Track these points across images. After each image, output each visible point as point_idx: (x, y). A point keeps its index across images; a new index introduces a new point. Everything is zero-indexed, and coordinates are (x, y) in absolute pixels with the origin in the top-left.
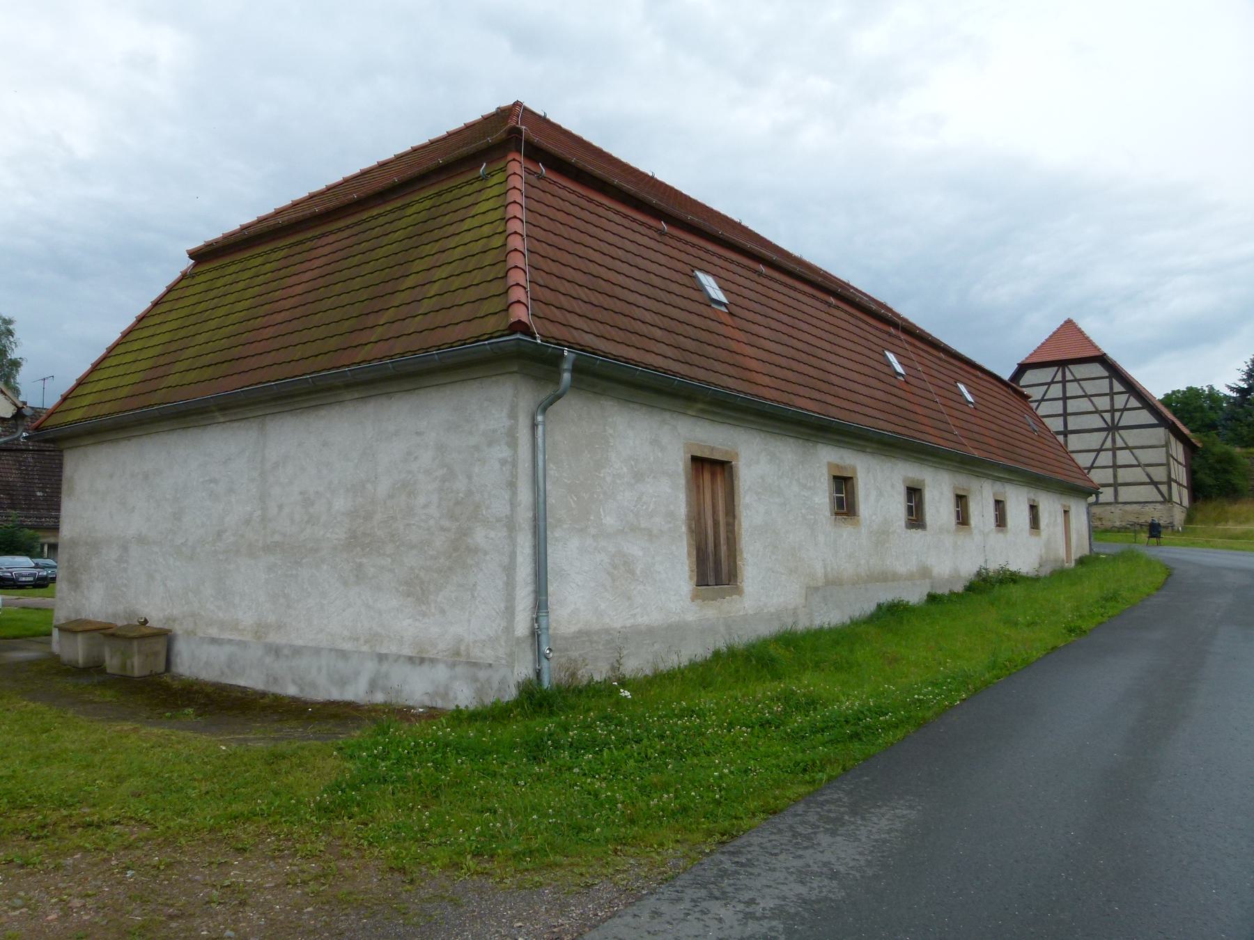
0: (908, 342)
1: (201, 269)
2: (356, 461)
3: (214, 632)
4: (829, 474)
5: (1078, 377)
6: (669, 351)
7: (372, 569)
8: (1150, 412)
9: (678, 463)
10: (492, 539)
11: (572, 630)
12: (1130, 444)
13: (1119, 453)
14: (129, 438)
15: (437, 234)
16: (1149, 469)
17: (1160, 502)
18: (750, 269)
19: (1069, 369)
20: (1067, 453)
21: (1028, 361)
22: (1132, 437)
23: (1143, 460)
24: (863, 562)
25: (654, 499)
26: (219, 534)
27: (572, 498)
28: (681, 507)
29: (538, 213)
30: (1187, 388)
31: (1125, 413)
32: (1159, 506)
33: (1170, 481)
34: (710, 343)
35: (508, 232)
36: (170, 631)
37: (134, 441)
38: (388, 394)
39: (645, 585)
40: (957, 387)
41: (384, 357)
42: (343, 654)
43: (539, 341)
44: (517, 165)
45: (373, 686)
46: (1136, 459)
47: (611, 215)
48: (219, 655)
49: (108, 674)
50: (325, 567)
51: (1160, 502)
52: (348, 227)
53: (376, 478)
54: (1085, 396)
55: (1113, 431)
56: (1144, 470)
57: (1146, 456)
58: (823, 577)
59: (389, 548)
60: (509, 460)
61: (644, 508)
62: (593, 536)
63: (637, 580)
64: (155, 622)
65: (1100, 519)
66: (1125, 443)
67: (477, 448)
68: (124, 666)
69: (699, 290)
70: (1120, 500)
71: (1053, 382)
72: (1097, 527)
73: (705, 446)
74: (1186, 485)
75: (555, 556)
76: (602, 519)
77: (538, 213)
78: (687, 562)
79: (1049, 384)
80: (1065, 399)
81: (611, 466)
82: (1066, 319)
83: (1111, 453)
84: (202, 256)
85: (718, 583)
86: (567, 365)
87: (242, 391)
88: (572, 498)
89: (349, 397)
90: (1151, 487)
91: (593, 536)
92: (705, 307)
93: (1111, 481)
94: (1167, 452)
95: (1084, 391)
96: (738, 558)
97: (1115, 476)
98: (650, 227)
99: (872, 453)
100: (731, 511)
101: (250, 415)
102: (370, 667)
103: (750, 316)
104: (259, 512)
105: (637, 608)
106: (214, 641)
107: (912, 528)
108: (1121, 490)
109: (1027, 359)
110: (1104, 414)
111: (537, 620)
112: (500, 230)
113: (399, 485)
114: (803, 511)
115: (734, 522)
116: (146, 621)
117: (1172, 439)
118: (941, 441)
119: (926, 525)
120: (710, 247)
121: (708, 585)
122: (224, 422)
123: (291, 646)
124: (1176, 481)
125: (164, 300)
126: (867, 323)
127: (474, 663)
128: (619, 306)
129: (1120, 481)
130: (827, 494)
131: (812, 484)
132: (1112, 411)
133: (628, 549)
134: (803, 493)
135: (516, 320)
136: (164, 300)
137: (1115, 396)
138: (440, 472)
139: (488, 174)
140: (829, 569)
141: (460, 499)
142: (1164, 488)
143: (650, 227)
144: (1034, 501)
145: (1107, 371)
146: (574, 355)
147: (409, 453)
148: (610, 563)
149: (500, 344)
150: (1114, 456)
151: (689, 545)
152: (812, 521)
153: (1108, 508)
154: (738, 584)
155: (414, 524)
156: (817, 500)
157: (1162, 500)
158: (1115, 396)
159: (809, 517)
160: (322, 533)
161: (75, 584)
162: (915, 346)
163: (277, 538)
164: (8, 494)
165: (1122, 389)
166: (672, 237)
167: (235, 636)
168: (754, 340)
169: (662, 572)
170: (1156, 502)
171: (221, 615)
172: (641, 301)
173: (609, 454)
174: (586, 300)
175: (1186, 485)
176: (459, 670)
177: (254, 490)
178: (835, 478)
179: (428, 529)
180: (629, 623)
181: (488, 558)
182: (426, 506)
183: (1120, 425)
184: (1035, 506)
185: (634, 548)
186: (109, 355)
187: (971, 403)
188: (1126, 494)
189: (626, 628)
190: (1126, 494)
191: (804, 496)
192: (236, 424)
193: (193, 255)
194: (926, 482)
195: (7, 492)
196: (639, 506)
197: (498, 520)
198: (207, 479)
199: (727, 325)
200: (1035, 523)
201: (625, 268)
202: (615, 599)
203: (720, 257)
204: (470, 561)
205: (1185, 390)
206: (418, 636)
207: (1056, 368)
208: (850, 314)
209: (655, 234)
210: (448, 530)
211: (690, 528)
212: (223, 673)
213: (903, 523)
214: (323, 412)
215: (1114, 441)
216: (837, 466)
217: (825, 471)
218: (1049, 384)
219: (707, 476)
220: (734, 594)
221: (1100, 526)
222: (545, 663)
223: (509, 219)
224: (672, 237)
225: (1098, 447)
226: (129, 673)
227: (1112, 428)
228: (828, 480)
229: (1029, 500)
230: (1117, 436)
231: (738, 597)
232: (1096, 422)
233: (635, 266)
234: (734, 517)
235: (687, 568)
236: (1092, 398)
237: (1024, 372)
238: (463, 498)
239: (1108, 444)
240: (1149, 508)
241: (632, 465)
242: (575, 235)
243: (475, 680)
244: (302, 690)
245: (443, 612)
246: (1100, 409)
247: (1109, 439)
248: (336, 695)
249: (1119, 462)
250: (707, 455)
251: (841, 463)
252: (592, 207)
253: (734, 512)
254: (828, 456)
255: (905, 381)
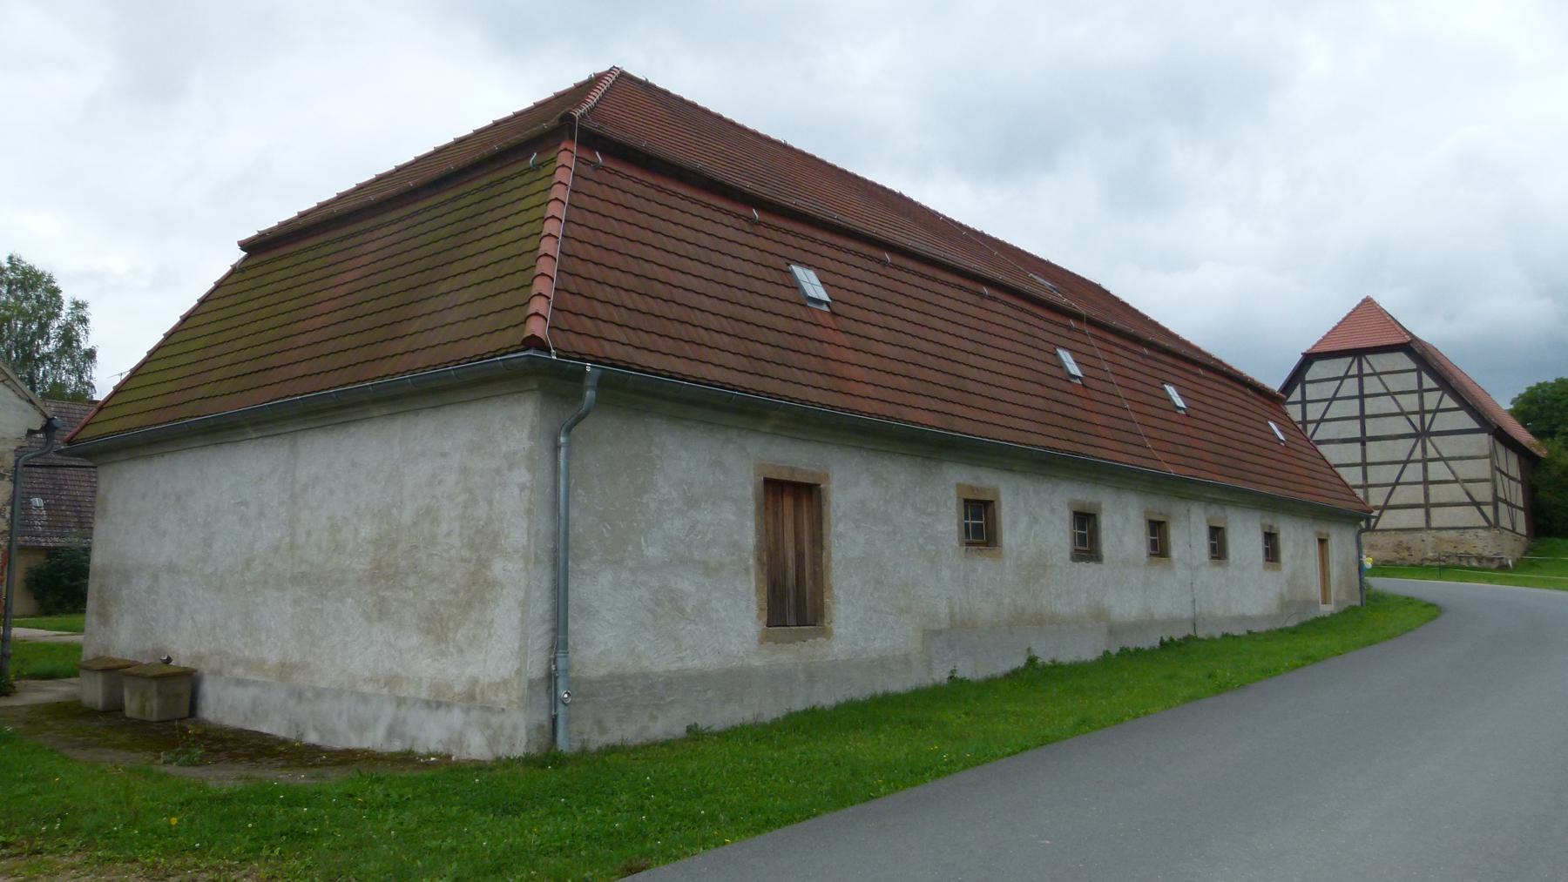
0: (1094, 336)
1: (256, 260)
2: (383, 483)
3: (239, 672)
4: (958, 498)
5: (1378, 370)
6: (732, 361)
7: (395, 604)
8: (1469, 414)
9: (745, 486)
10: (509, 571)
11: (601, 673)
12: (1445, 455)
13: (1430, 465)
14: (162, 455)
15: (481, 232)
16: (1468, 486)
17: (1483, 528)
18: (872, 259)
19: (1366, 359)
20: (1331, 468)
21: (1314, 351)
22: (1447, 446)
23: (1462, 475)
24: (1007, 601)
25: (712, 528)
26: (248, 564)
27: (605, 527)
28: (749, 537)
29: (587, 210)
30: (1557, 380)
31: (1439, 415)
32: (1482, 533)
33: (1496, 500)
34: (797, 349)
35: (543, 234)
36: (196, 671)
37: (167, 457)
38: (416, 411)
39: (697, 625)
40: (1164, 389)
41: (428, 367)
42: (364, 698)
43: (555, 358)
44: (567, 158)
45: (391, 733)
46: (1453, 473)
47: (685, 205)
48: (244, 696)
49: (126, 718)
50: (350, 600)
51: (1483, 528)
52: (400, 220)
53: (402, 503)
54: (1388, 393)
55: (1423, 437)
56: (1462, 486)
57: (1466, 470)
58: (948, 618)
59: (412, 581)
60: (528, 484)
61: (699, 537)
62: (631, 569)
63: (687, 619)
64: (182, 660)
65: (1408, 549)
66: (1439, 453)
67: (498, 471)
68: (142, 709)
69: (793, 287)
70: (1433, 524)
71: (1346, 376)
72: (1403, 559)
73: (783, 467)
74: (1522, 506)
75: (580, 590)
76: (642, 551)
77: (587, 210)
78: (754, 598)
79: (1342, 379)
80: (1362, 397)
81: (657, 491)
82: (1364, 297)
83: (1420, 465)
84: (256, 247)
85: (801, 622)
86: (589, 383)
87: (269, 406)
88: (605, 527)
89: (376, 413)
90: (1473, 509)
91: (631, 569)
92: (799, 307)
93: (1422, 501)
94: (1492, 463)
95: (1386, 388)
96: (826, 595)
97: (1426, 495)
98: (738, 216)
99: (1024, 473)
100: (818, 541)
101: (283, 431)
102: (389, 711)
103: (856, 313)
104: (288, 539)
105: (686, 650)
106: (240, 682)
107: (1082, 561)
108: (1434, 512)
109: (1314, 347)
110: (1412, 417)
111: (555, 660)
112: (537, 231)
113: (424, 510)
114: (921, 541)
115: (822, 553)
116: (169, 660)
117: (1501, 449)
118: (1123, 458)
119: (1102, 556)
120: (819, 235)
121: (786, 626)
122: (257, 438)
123: (314, 688)
124: (1505, 501)
125: (211, 298)
126: (1037, 316)
127: (489, 707)
128: (674, 311)
129: (1432, 500)
130: (955, 521)
131: (934, 509)
132: (1422, 412)
133: (676, 584)
134: (920, 520)
135: (529, 334)
136: (211, 298)
137: (1425, 394)
138: (463, 498)
139: (540, 165)
140: (957, 609)
141: (480, 527)
142: (1488, 510)
143: (738, 216)
144: (1271, 527)
145: (1415, 362)
146: (599, 371)
147: (434, 476)
148: (652, 600)
149: (512, 360)
150: (1425, 469)
151: (758, 580)
152: (933, 553)
153: (1418, 535)
154: (826, 624)
155: (436, 555)
156: (940, 527)
157: (1486, 524)
158: (1425, 394)
159: (928, 548)
160: (348, 562)
161: (104, 617)
162: (1106, 341)
163: (304, 568)
164: (75, 511)
165: (1434, 385)
166: (769, 226)
167: (261, 678)
168: (862, 343)
169: (721, 610)
170: (1479, 528)
171: (247, 653)
172: (707, 303)
173: (655, 478)
174: (631, 306)
175: (1522, 506)
176: (474, 715)
177: (284, 514)
178: (967, 502)
179: (449, 560)
180: (674, 667)
181: (505, 592)
182: (448, 535)
183: (1431, 430)
184: (1274, 534)
185: (685, 584)
186: (151, 359)
187: (1181, 408)
188: (1440, 517)
189: (670, 671)
190: (1440, 517)
191: (923, 523)
192: (267, 441)
193: (244, 245)
194: (1103, 506)
195: (74, 509)
196: (692, 536)
197: (516, 551)
198: (237, 501)
199: (825, 327)
200: (1272, 552)
201: (693, 267)
202: (657, 640)
203: (831, 246)
204: (488, 596)
205: (1554, 382)
206: (435, 678)
207: (1350, 359)
208: (1012, 306)
209: (745, 224)
210: (469, 561)
211: (759, 560)
212: (246, 719)
213: (1067, 556)
214: (352, 429)
215: (1424, 450)
216: (971, 488)
217: (953, 493)
218: (1342, 379)
219: (788, 502)
220: (820, 636)
221: (1407, 557)
222: (561, 709)
223: (548, 218)
224: (769, 226)
225: (1405, 458)
226: (147, 717)
227: (1423, 434)
228: (957, 505)
229: (1263, 526)
230: (1429, 445)
231: (825, 640)
232: (1402, 426)
233: (708, 263)
234: (822, 548)
235: (754, 606)
236: (1396, 396)
237: (1311, 363)
238: (483, 527)
239: (1418, 454)
240: (1469, 535)
241: (684, 489)
242: (632, 232)
243: (489, 726)
244: (323, 737)
245: (461, 651)
246: (1406, 410)
247: (1419, 448)
248: (354, 742)
249: (1431, 477)
250: (785, 476)
251: (975, 483)
252: (661, 197)
253: (821, 542)
254: (955, 478)
255: (1083, 385)
